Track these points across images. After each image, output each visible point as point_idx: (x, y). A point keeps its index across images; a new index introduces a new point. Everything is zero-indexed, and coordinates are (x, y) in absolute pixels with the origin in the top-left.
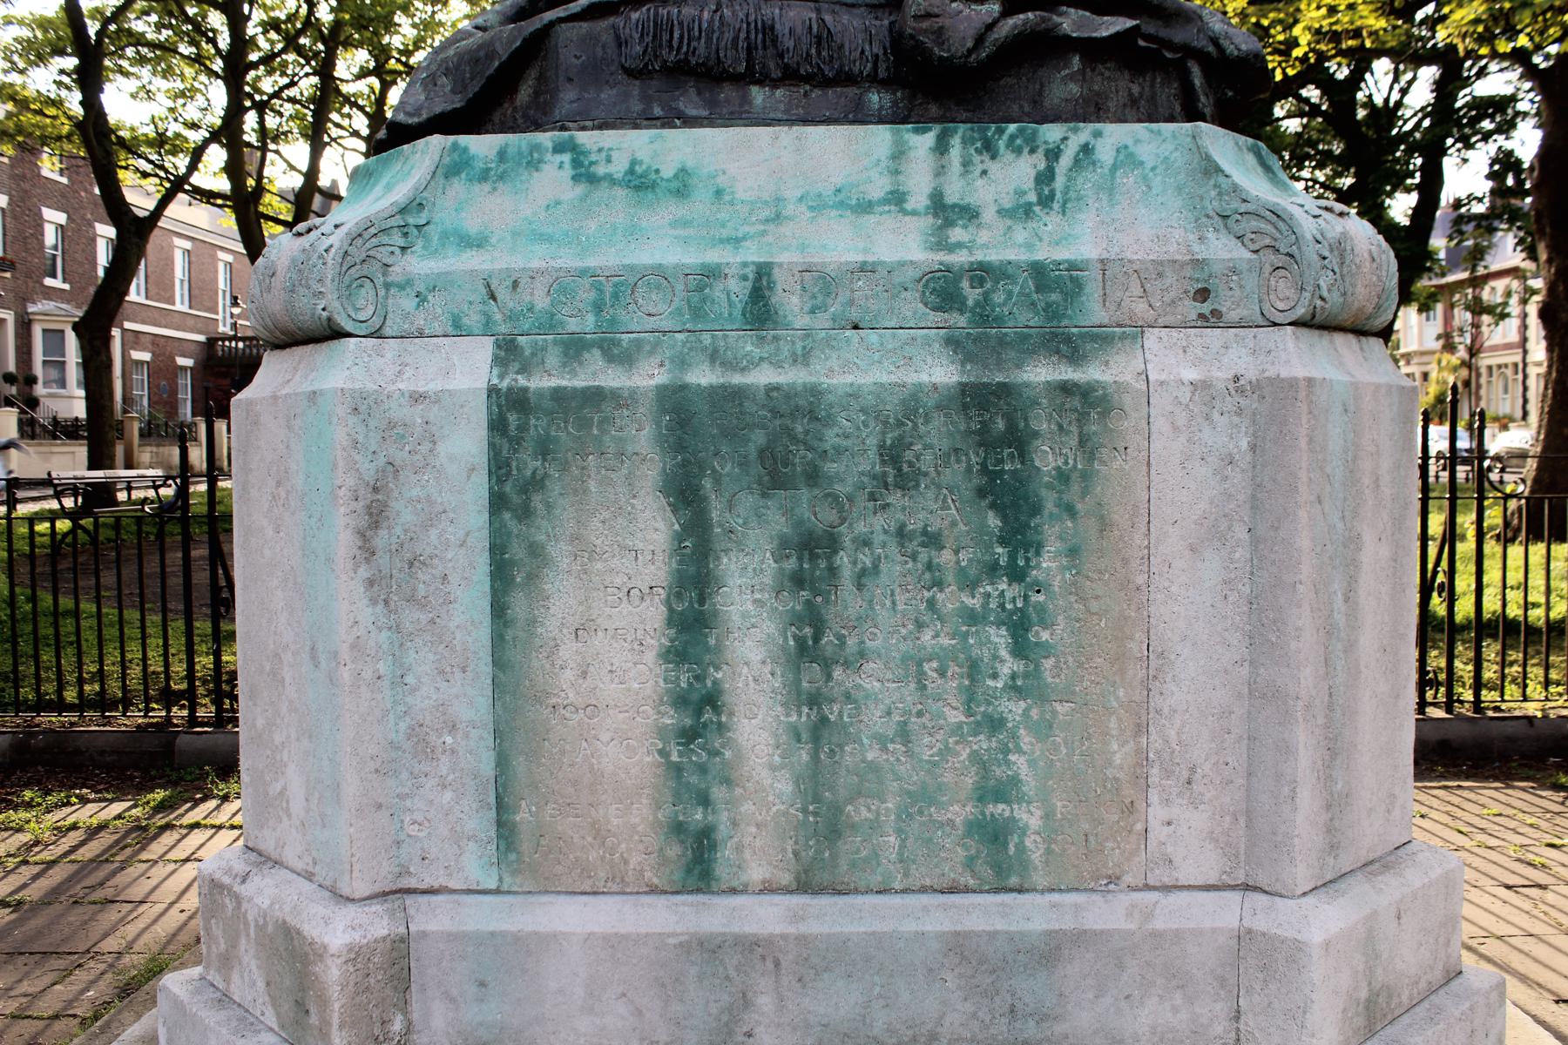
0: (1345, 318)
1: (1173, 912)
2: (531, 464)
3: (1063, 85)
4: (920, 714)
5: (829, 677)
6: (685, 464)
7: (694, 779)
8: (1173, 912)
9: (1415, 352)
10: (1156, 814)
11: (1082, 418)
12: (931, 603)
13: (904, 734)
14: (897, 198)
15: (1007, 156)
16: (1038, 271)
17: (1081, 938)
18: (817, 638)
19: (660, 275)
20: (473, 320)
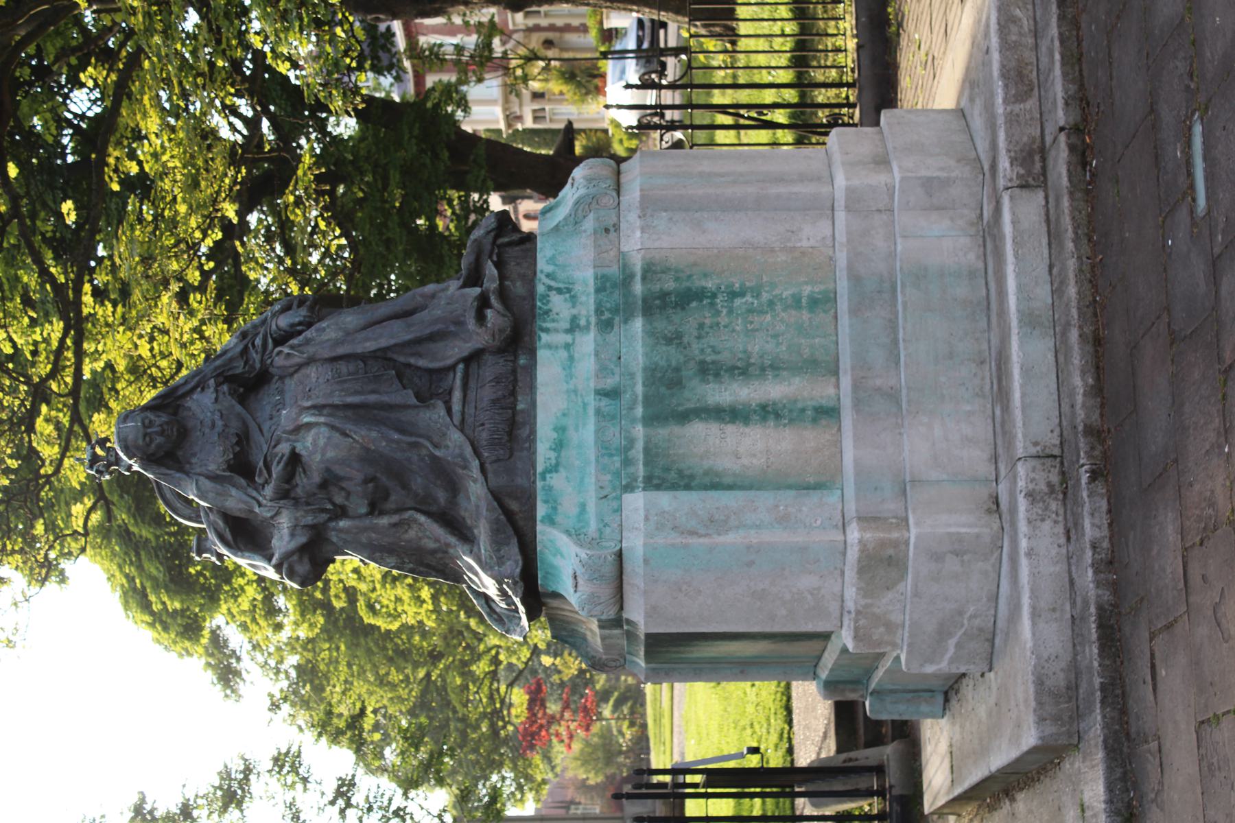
1: (841, 237)
2: (673, 475)
3: (518, 288)
4: (768, 330)
5: (754, 364)
7: (795, 414)
8: (841, 237)
9: (505, 110)
10: (805, 244)
11: (655, 272)
12: (725, 327)
13: (776, 336)
15: (550, 306)
17: (850, 267)
18: (738, 368)
19: (599, 431)
20: (615, 504)
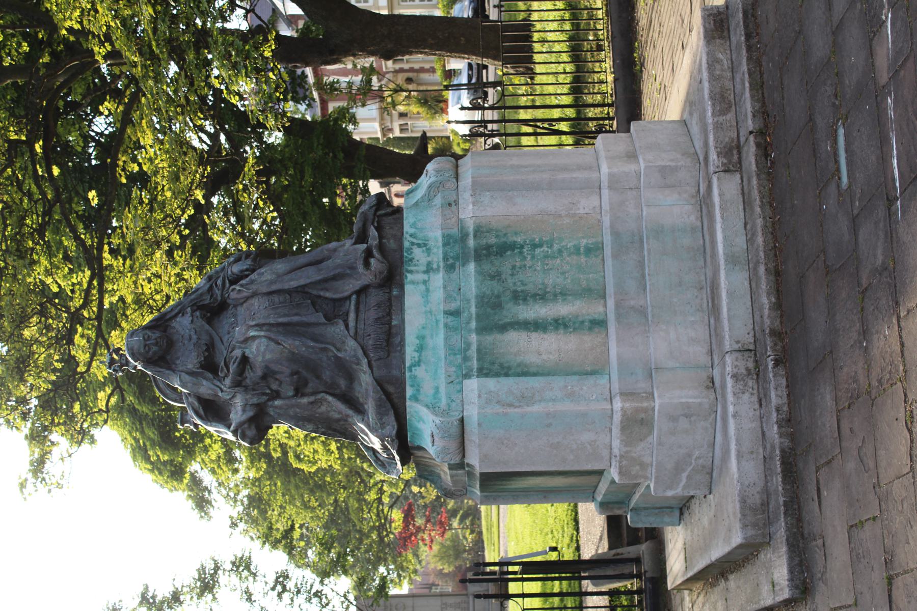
0: (455, 170)
1: (606, 206)
3: (391, 244)
6: (496, 328)
7: (577, 325)
8: (606, 206)
11: (482, 232)
12: (529, 267)
13: (563, 273)
14: (425, 282)
16: (445, 245)
18: (539, 295)
20: (458, 387)
